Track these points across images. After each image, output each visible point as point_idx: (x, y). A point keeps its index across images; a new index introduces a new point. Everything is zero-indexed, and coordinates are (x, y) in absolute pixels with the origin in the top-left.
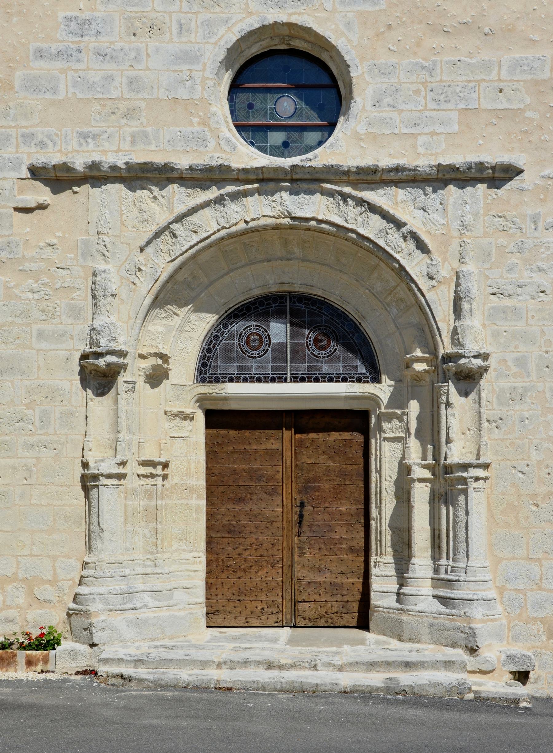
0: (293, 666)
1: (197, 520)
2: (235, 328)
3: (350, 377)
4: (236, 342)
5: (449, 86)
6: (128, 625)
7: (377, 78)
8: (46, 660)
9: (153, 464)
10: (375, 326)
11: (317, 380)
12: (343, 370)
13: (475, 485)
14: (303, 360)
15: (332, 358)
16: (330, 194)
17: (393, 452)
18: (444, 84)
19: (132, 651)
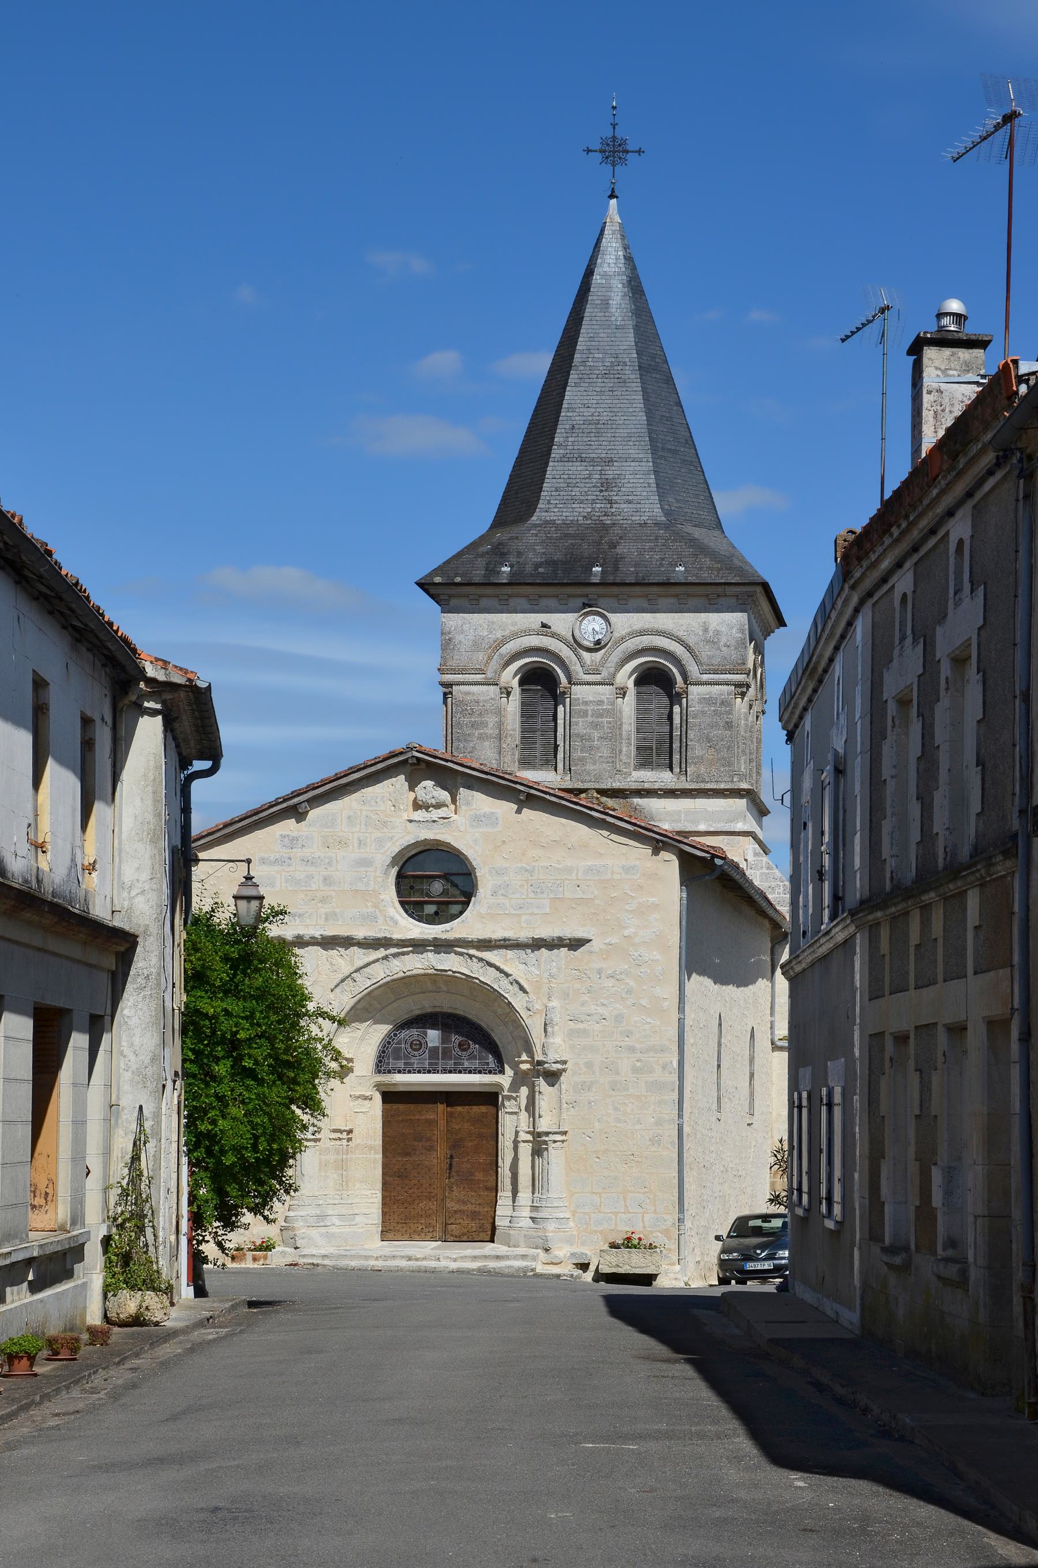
0: (425, 1259)
1: (375, 1168)
8: (265, 1257)
9: (341, 1132)
10: (499, 1035)
11: (460, 1072)
13: (554, 1145)
15: (471, 1057)
16: (461, 954)
17: (512, 1123)
19: (323, 1252)
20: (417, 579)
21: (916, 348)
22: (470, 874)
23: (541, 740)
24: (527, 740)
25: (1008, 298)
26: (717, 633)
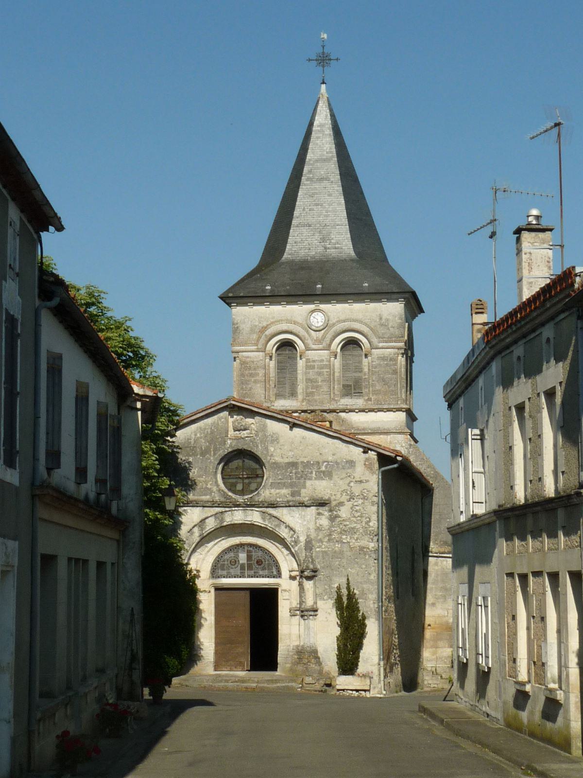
4: (226, 563)
14: (252, 570)
20: (219, 295)
21: (518, 231)
23: (285, 380)
24: (280, 383)
25: (561, 205)
26: (387, 320)
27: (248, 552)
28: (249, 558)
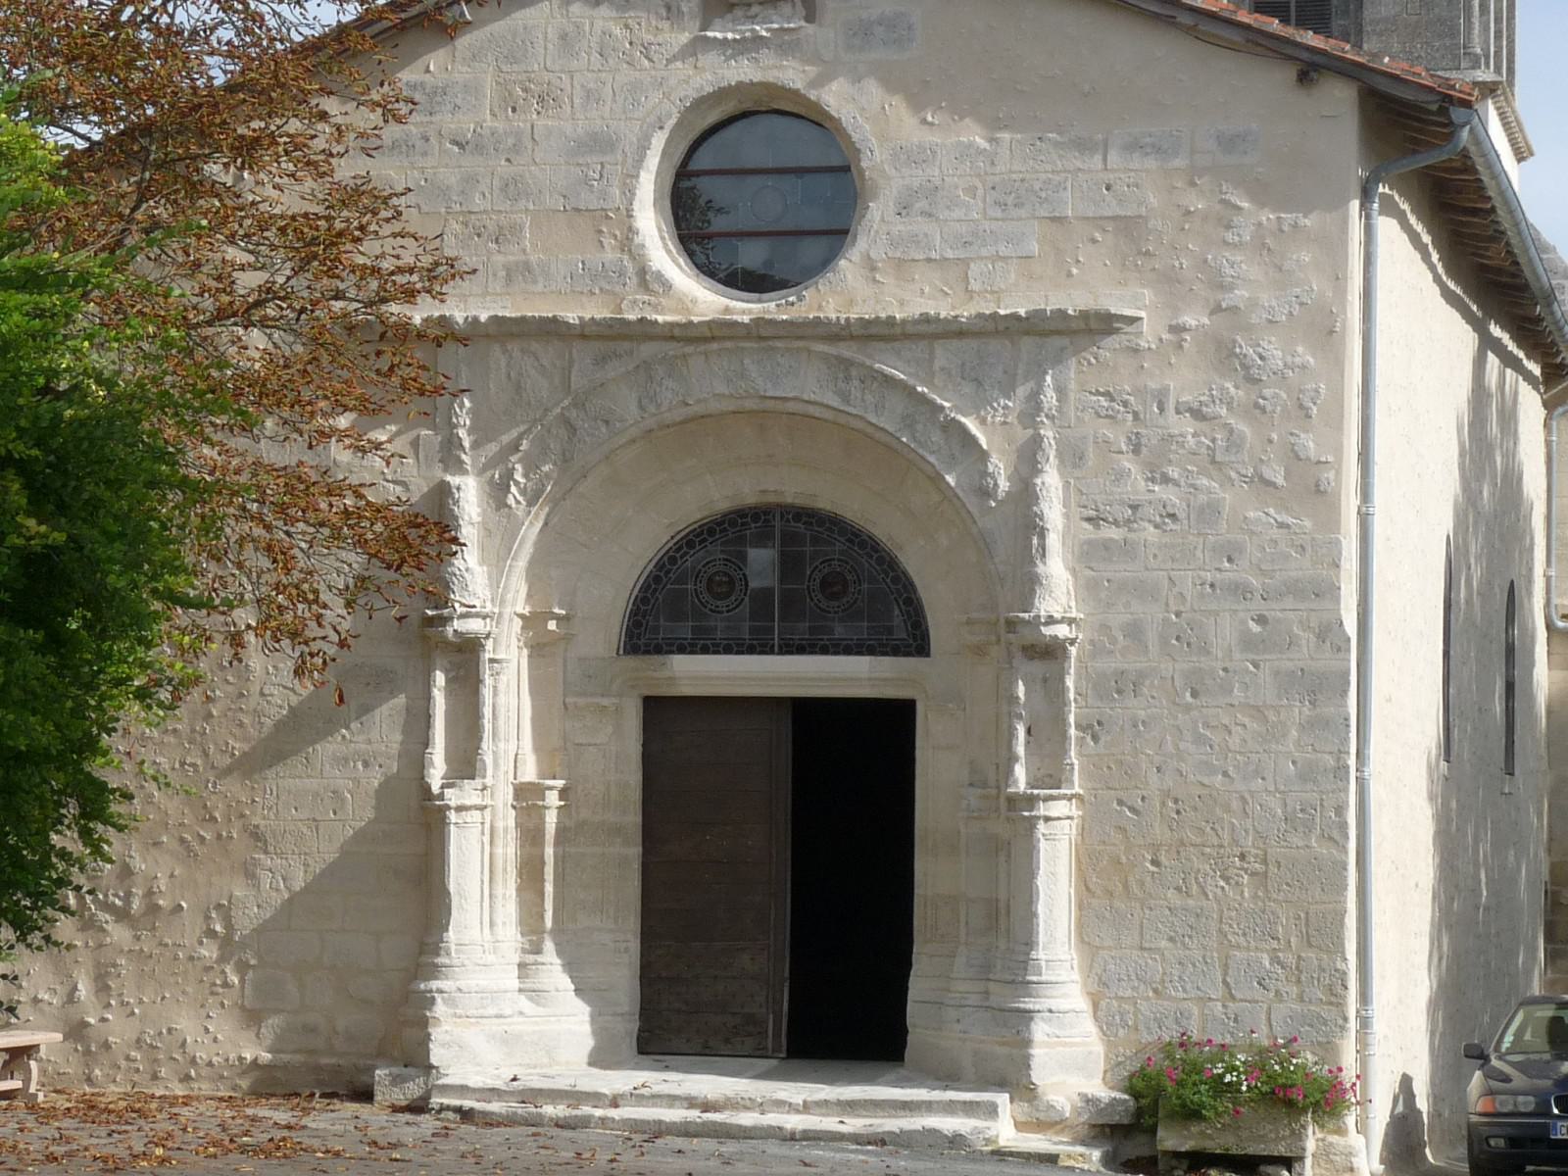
2: (688, 564)
3: (880, 645)
5: (1022, 180)
6: (488, 1042)
7: (904, 170)
12: (868, 634)
18: (1014, 176)
22: (846, 169)
27: (789, 539)
28: (790, 565)
